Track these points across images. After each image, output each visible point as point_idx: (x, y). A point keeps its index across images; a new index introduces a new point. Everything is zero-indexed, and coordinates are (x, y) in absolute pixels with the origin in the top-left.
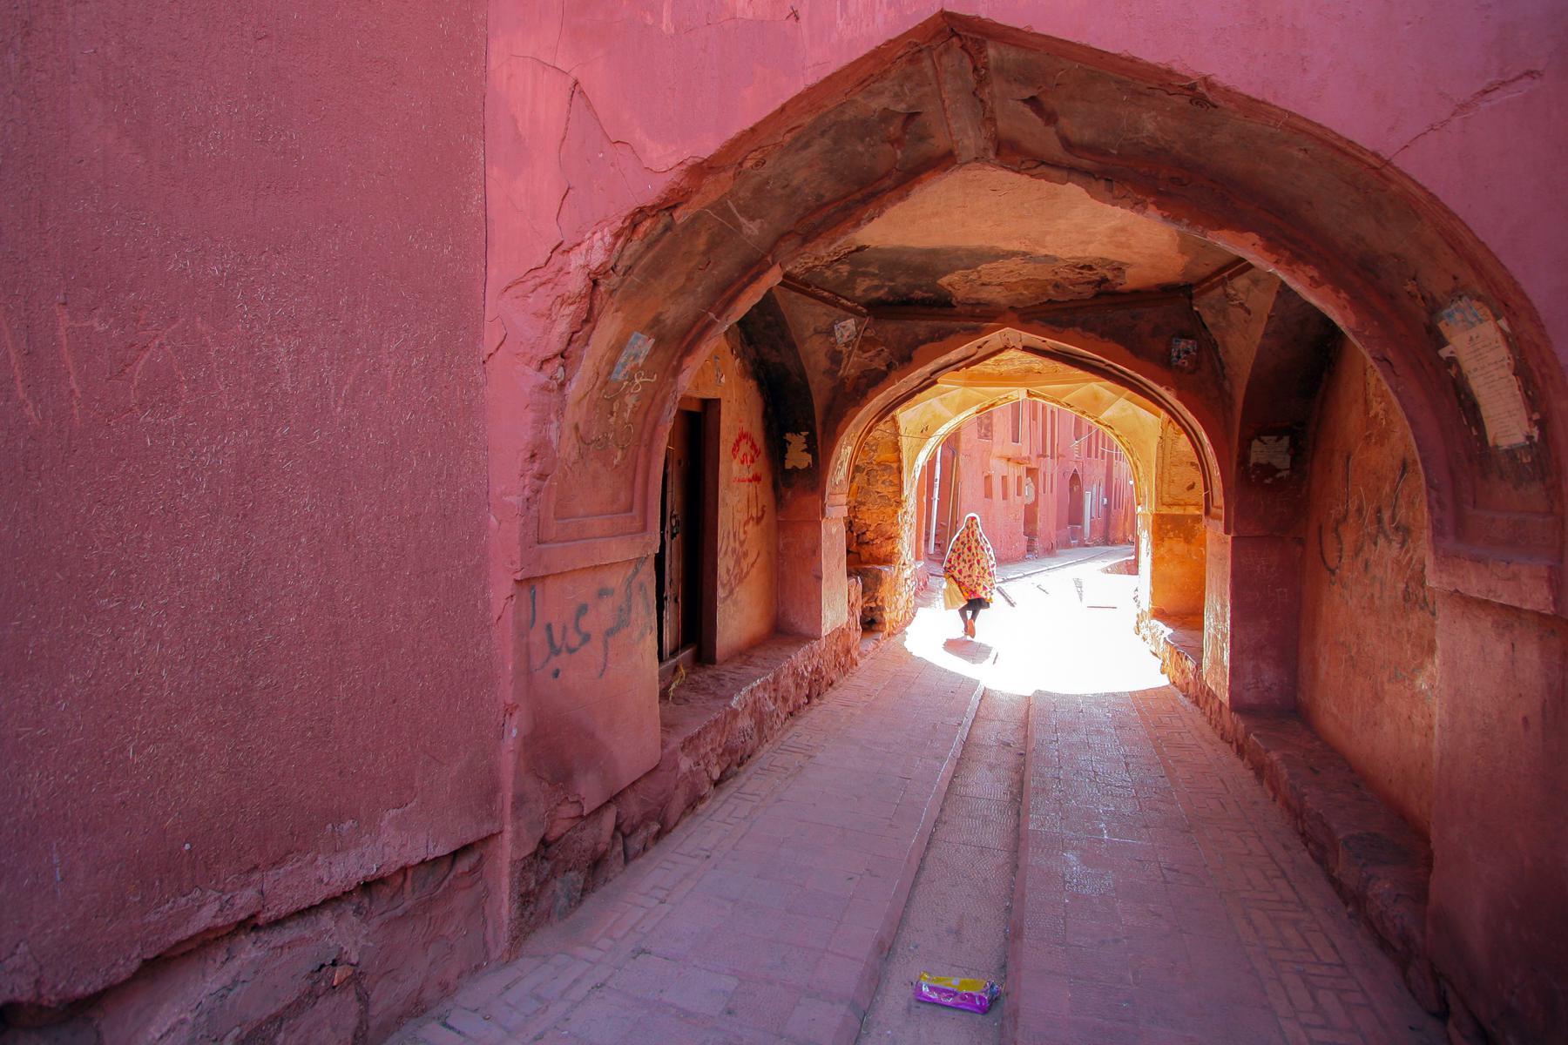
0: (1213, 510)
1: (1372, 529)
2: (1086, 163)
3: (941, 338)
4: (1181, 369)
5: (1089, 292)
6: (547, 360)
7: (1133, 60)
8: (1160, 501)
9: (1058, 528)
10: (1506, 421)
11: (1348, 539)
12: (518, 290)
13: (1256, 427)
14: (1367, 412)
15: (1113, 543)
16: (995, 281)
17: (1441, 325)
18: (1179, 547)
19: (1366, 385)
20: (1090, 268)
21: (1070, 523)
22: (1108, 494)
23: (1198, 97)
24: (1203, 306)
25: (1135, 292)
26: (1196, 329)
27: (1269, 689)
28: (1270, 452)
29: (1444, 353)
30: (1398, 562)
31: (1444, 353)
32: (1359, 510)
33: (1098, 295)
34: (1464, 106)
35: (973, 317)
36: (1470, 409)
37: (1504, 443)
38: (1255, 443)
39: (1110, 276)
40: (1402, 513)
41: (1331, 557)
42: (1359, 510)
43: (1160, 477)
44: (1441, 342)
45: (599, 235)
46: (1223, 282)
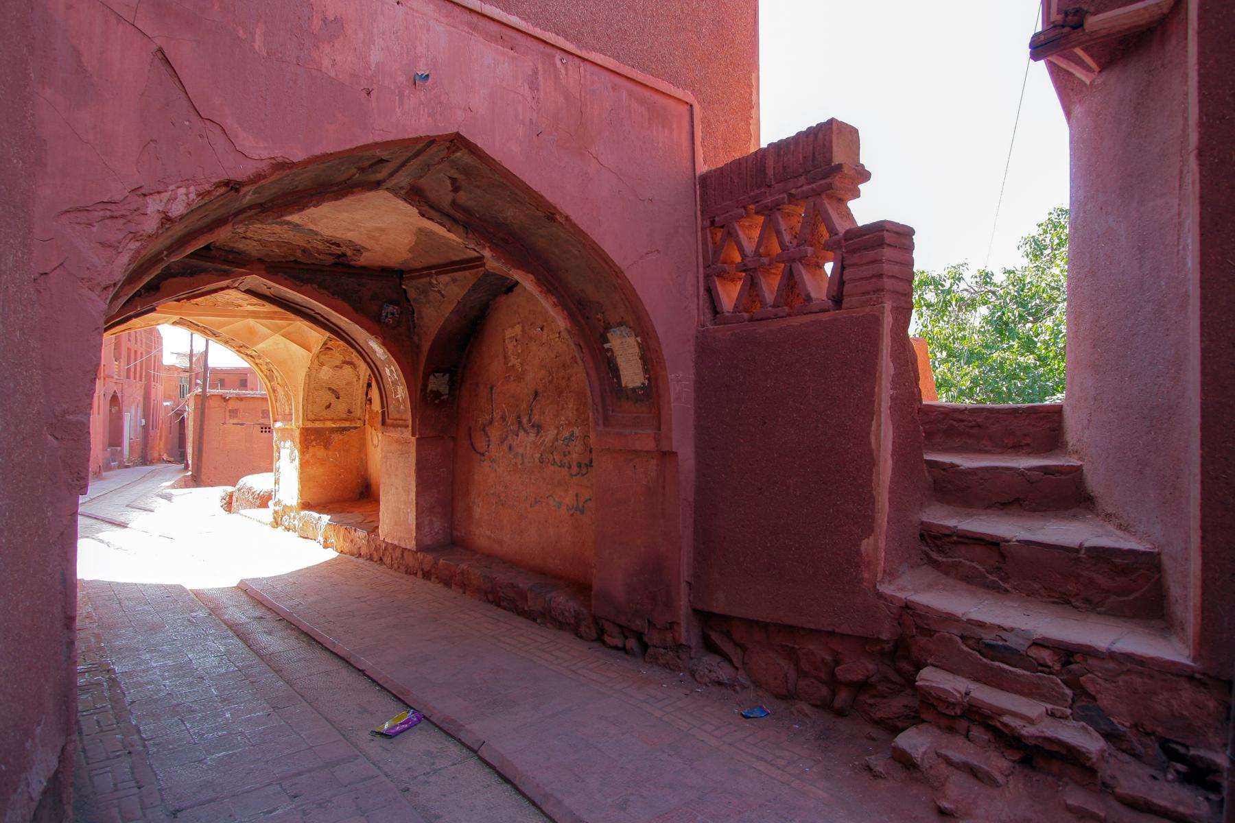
0: (388, 421)
1: (514, 427)
2: (458, 215)
3: (192, 274)
4: (387, 325)
5: (330, 260)
6: (109, 286)
7: (542, 197)
8: (306, 418)
9: (104, 449)
10: (632, 375)
11: (494, 434)
12: (82, 217)
13: (434, 368)
14: (506, 363)
15: (151, 463)
16: (256, 237)
17: (609, 335)
18: (320, 452)
19: (505, 348)
20: (338, 245)
21: (110, 445)
22: (146, 414)
23: (551, 214)
24: (411, 288)
25: (364, 268)
26: (402, 299)
27: (437, 533)
28: (438, 383)
29: (606, 346)
30: (534, 443)
31: (606, 346)
32: (503, 418)
33: (335, 264)
34: (642, 257)
35: (227, 262)
36: (615, 371)
37: (631, 386)
38: (432, 377)
39: (349, 253)
40: (536, 418)
41: (481, 444)
42: (503, 418)
43: (306, 399)
44: (607, 341)
45: (183, 190)
46: (430, 275)
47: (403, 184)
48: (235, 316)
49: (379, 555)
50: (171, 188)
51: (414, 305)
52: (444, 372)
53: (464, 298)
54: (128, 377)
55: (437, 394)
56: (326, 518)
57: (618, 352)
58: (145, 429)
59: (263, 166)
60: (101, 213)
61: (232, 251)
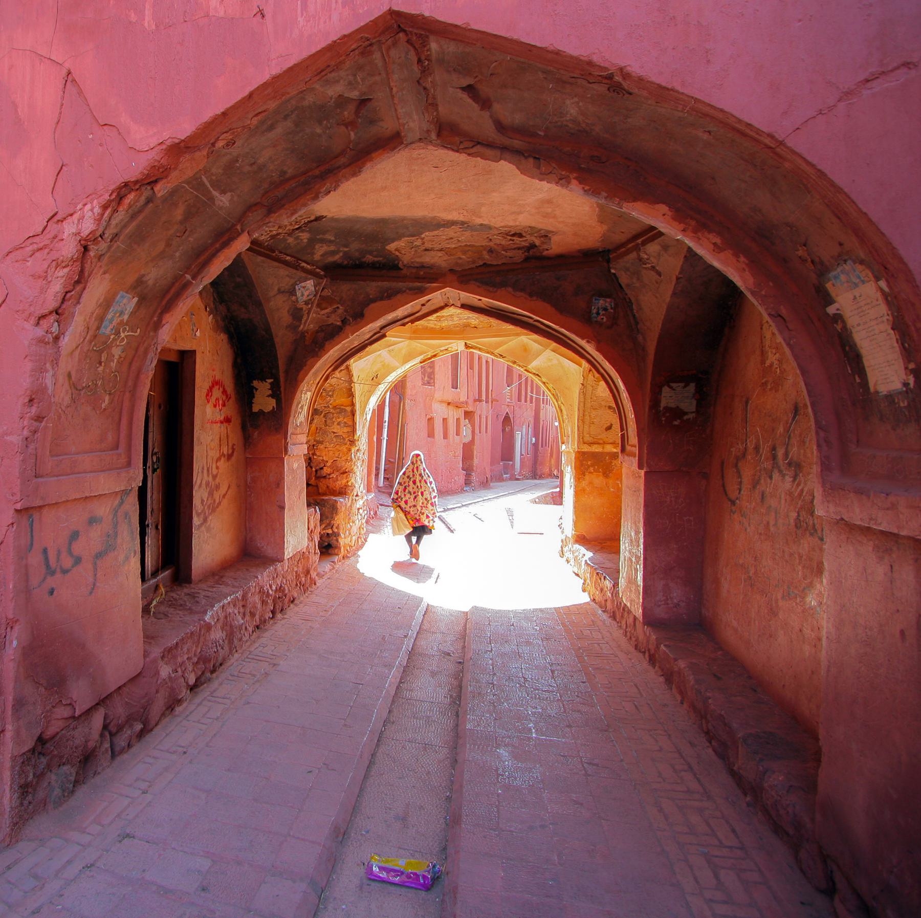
1: (767, 465)
2: (517, 143)
3: (389, 297)
4: (600, 324)
5: (519, 256)
7: (558, 53)
8: (582, 440)
11: (747, 474)
12: (18, 254)
14: (763, 362)
15: (541, 477)
18: (598, 480)
19: (762, 338)
20: (520, 235)
23: (615, 85)
25: (560, 257)
26: (612, 287)
29: (831, 310)
32: (757, 448)
33: (527, 259)
37: (883, 389)
38: (665, 389)
39: (537, 243)
42: (757, 448)
43: (582, 420)
44: (829, 301)
45: (88, 207)
46: (637, 248)
47: (425, 126)
48: (509, 335)
49: (618, 612)
50: (78, 208)
51: (628, 292)
52: (686, 381)
53: (682, 271)
54: (519, 400)
55: (677, 413)
56: (589, 554)
57: (852, 320)
58: (535, 445)
59: (154, 155)
60: (31, 248)
61: (422, 266)
